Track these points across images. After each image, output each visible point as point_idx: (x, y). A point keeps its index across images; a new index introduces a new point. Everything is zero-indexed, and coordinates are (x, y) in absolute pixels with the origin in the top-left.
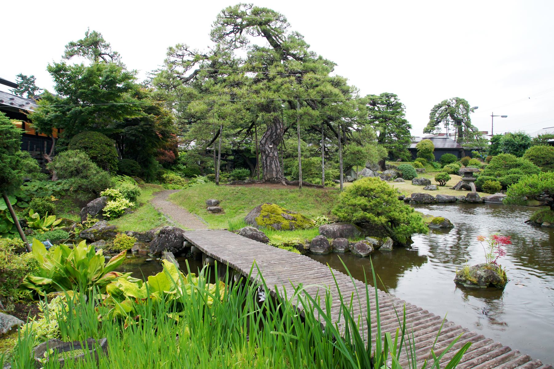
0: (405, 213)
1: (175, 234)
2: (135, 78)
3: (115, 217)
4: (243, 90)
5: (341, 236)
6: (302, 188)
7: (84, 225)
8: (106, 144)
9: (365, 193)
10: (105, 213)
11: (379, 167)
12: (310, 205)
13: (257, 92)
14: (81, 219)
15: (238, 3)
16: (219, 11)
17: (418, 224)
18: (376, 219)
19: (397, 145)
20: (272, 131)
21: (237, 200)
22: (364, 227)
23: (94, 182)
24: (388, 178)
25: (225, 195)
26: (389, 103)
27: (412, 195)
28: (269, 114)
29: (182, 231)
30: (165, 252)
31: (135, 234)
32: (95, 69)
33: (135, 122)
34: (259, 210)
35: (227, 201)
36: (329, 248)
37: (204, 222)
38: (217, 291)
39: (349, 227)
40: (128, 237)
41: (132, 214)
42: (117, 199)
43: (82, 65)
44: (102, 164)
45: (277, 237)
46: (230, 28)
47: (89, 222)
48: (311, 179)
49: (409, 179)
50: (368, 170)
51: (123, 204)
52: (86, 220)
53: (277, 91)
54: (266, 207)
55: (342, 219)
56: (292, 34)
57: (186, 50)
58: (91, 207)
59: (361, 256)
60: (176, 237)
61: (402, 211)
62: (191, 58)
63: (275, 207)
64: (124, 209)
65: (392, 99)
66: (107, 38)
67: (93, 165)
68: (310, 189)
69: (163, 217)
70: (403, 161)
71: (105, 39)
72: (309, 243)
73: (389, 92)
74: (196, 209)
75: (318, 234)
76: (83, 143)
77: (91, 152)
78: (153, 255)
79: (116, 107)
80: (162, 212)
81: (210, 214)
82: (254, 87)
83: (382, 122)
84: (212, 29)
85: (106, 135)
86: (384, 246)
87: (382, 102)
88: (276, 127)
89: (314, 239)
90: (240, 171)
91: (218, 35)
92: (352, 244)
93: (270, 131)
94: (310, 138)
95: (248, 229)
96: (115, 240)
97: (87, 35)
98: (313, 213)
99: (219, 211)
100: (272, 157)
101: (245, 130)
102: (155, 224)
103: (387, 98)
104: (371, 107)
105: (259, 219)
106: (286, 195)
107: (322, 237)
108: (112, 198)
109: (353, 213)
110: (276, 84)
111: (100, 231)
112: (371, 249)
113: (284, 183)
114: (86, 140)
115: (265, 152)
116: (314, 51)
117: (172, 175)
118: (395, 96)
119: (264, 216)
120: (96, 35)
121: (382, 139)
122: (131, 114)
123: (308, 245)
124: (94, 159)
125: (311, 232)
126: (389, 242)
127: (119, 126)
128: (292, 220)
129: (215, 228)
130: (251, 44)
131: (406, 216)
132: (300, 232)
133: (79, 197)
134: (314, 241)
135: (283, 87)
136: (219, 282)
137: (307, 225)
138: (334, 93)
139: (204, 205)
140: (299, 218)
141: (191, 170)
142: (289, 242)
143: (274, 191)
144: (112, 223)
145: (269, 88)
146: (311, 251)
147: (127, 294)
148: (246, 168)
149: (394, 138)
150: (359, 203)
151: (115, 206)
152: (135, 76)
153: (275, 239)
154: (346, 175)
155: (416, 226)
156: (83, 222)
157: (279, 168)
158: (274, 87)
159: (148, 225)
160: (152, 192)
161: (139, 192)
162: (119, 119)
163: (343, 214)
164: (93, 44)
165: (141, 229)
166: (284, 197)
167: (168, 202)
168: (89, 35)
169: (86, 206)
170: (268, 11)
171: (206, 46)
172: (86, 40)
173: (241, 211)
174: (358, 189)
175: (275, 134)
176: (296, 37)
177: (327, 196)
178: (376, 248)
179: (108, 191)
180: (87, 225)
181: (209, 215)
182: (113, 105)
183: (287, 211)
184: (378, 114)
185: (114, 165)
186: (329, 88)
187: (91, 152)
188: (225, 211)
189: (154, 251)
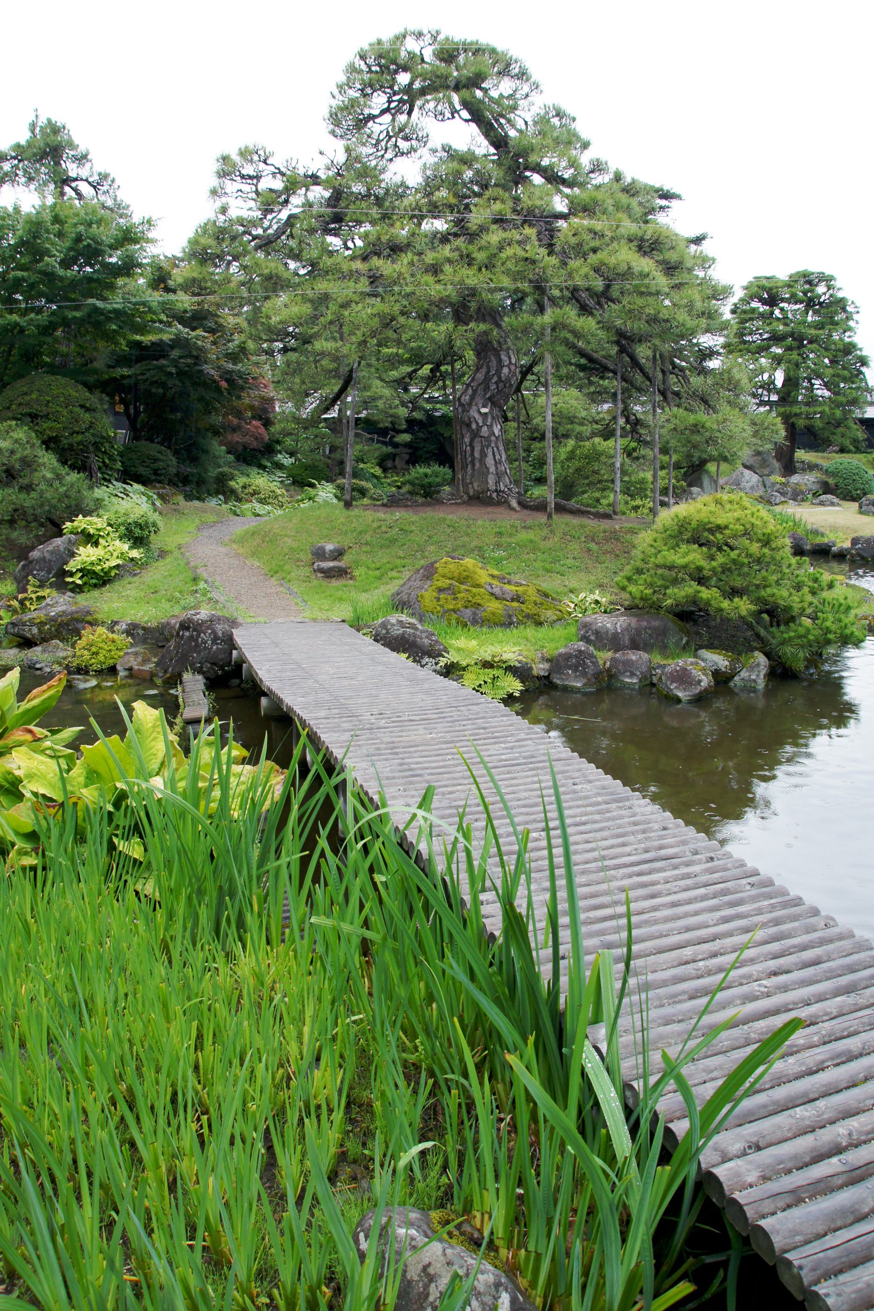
0: (806, 590)
1: (214, 632)
2: (148, 241)
3: (95, 586)
4: (403, 264)
5: (635, 645)
6: (554, 517)
7: (22, 602)
8: (82, 406)
9: (700, 535)
10: (72, 574)
11: (776, 465)
12: (570, 562)
13: (435, 270)
14: (18, 588)
15: (399, 30)
16: (350, 56)
17: (840, 621)
18: (725, 604)
19: (827, 409)
20: (488, 372)
21: (389, 547)
22: (693, 622)
23: (48, 501)
24: (797, 496)
25: (360, 533)
26: (811, 300)
27: (855, 541)
28: (465, 328)
29: (234, 623)
30: (187, 676)
31: (132, 630)
32: (47, 217)
33: (158, 350)
34: (429, 572)
35: (365, 548)
36: (598, 675)
37: (299, 600)
38: (254, 783)
39: (656, 623)
40: (111, 636)
41: (136, 579)
42: (101, 540)
43: (17, 210)
44: (74, 457)
45: (465, 646)
46: (379, 101)
47: (34, 596)
48: (597, 495)
49: (853, 499)
50: (747, 472)
51: (115, 554)
52: (26, 591)
53: (489, 266)
54: (446, 565)
55: (637, 601)
56: (542, 112)
57: (265, 162)
58: (38, 561)
59: (678, 700)
60: (215, 639)
61: (798, 587)
62: (278, 184)
63: (470, 566)
64: (118, 567)
65: (821, 289)
66: (81, 135)
67: (48, 459)
68: (575, 521)
69: (202, 585)
70: (842, 450)
71: (76, 140)
72: (548, 660)
73: (814, 267)
74: (286, 567)
75: (575, 639)
76: (28, 404)
77: (45, 426)
78: (164, 682)
79: (102, 314)
80: (205, 575)
81: (318, 581)
82: (430, 257)
83: (789, 349)
84: (335, 103)
85: (85, 384)
86: (744, 674)
87: (793, 295)
88: (500, 361)
89: (562, 650)
90: (428, 471)
91: (349, 119)
92: (660, 666)
93: (484, 370)
94: (592, 389)
95: (394, 621)
96: (81, 643)
97: (33, 131)
98: (574, 584)
99: (341, 573)
100: (488, 439)
101: (426, 370)
102: (183, 602)
103: (807, 287)
104: (762, 308)
105: (428, 596)
106: (511, 535)
107: (582, 646)
108: (91, 539)
109: (667, 588)
110: (487, 248)
111: (53, 620)
112: (706, 681)
113: (514, 503)
114: (34, 396)
115: (469, 425)
116: (603, 159)
117: (261, 481)
118: (828, 280)
119: (440, 590)
120: (55, 129)
121: (789, 394)
122: (142, 329)
123: (547, 666)
124: (49, 443)
125: (559, 632)
126: (758, 665)
127: (122, 360)
128: (513, 600)
129: (320, 615)
130: (436, 142)
131: (809, 598)
132: (530, 632)
133: (14, 535)
134: (560, 655)
135: (503, 255)
136: (265, 764)
137: (549, 613)
138: (636, 270)
139: (307, 557)
140: (532, 594)
141: (307, 468)
142: (493, 656)
143: (482, 523)
144: (84, 600)
145: (468, 260)
146: (551, 682)
147: (28, 789)
148: (442, 463)
149: (819, 392)
150: (681, 561)
151: (94, 558)
152: (150, 235)
153: (459, 650)
154: (690, 485)
155: (833, 628)
156: (20, 596)
157: (505, 466)
158: (480, 256)
159: (165, 605)
160: (197, 522)
161: (154, 524)
162: (117, 343)
163: (642, 588)
164: (47, 152)
165: (149, 614)
166: (504, 540)
167: (223, 550)
168: (37, 130)
169: (26, 558)
170: (478, 51)
171: (312, 147)
172: (30, 144)
173: (394, 574)
174: (683, 525)
175: (495, 379)
176: (556, 121)
177: (617, 539)
178: (722, 679)
179: (81, 522)
180: (28, 603)
181: (315, 583)
182: (96, 309)
183: (501, 579)
184: (781, 327)
185: (111, 458)
186: (625, 256)
187: (45, 426)
188: (356, 573)
189: (166, 672)
